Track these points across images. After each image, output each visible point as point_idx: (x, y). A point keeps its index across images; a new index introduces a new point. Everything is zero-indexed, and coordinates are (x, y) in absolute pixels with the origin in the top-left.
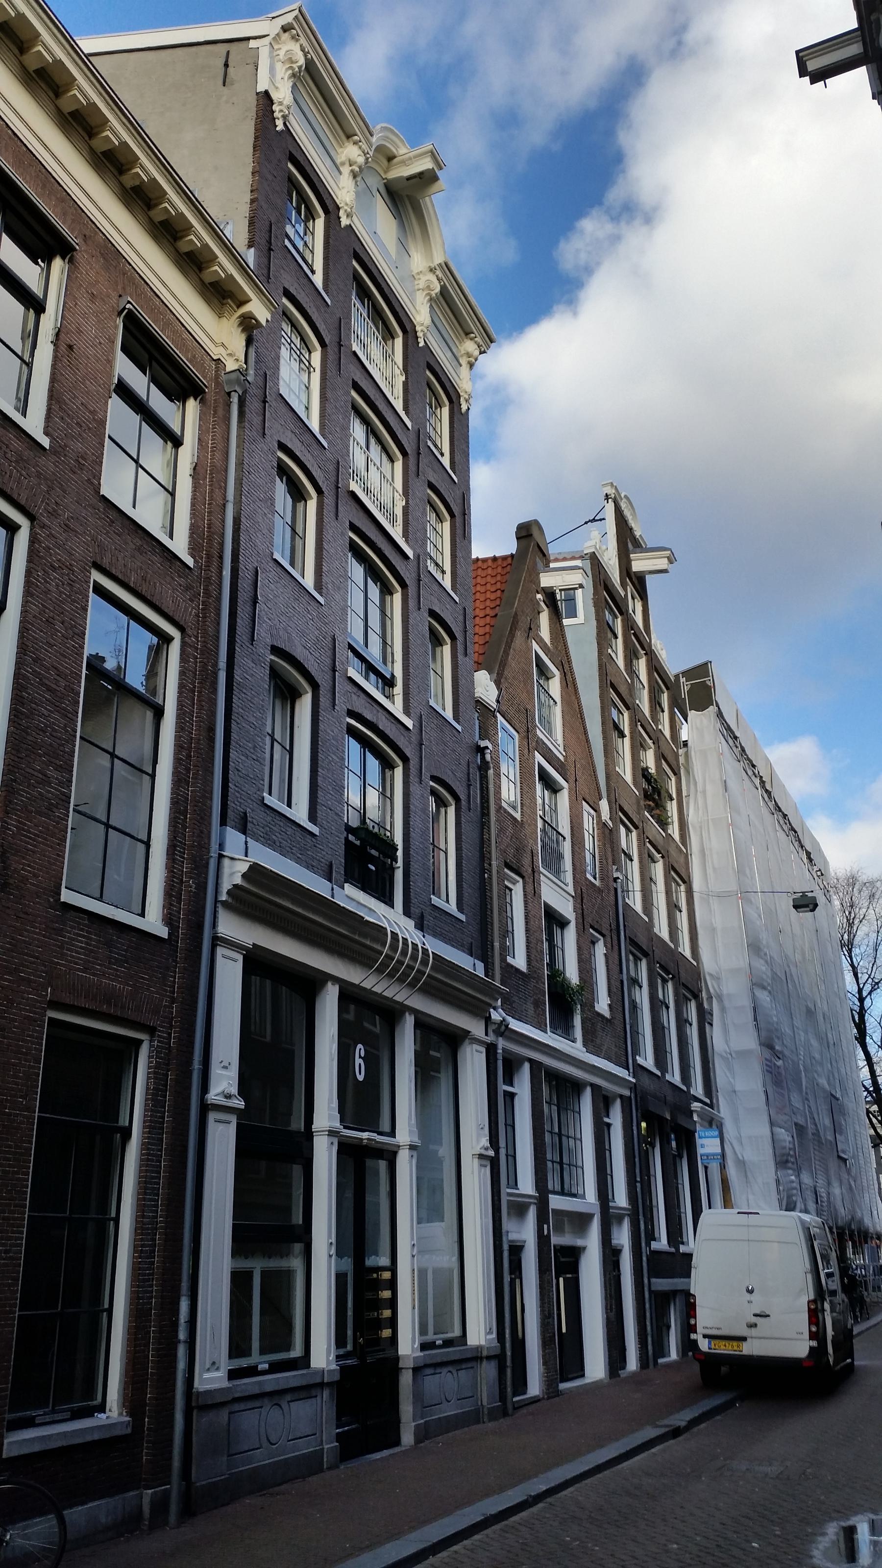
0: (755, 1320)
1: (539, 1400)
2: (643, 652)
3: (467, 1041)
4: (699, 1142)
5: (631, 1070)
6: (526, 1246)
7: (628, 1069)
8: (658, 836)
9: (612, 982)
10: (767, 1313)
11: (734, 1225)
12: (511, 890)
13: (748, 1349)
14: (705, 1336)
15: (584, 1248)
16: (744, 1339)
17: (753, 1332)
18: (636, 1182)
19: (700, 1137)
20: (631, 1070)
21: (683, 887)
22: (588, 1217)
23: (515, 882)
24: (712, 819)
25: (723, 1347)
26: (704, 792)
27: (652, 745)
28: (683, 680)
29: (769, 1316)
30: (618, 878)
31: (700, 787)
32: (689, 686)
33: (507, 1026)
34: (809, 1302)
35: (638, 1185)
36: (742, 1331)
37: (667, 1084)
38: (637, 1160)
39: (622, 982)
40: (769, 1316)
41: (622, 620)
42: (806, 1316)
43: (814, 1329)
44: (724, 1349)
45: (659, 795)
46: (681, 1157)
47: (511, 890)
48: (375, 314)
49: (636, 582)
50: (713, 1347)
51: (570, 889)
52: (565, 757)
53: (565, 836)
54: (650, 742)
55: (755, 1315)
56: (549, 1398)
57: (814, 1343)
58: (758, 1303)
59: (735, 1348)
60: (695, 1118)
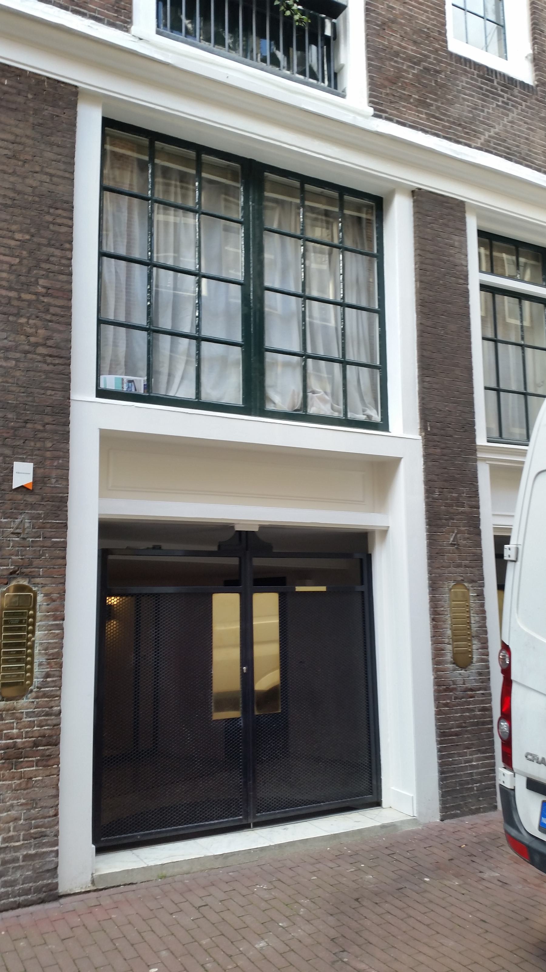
14: (533, 785)
15: (385, 532)
22: (381, 472)
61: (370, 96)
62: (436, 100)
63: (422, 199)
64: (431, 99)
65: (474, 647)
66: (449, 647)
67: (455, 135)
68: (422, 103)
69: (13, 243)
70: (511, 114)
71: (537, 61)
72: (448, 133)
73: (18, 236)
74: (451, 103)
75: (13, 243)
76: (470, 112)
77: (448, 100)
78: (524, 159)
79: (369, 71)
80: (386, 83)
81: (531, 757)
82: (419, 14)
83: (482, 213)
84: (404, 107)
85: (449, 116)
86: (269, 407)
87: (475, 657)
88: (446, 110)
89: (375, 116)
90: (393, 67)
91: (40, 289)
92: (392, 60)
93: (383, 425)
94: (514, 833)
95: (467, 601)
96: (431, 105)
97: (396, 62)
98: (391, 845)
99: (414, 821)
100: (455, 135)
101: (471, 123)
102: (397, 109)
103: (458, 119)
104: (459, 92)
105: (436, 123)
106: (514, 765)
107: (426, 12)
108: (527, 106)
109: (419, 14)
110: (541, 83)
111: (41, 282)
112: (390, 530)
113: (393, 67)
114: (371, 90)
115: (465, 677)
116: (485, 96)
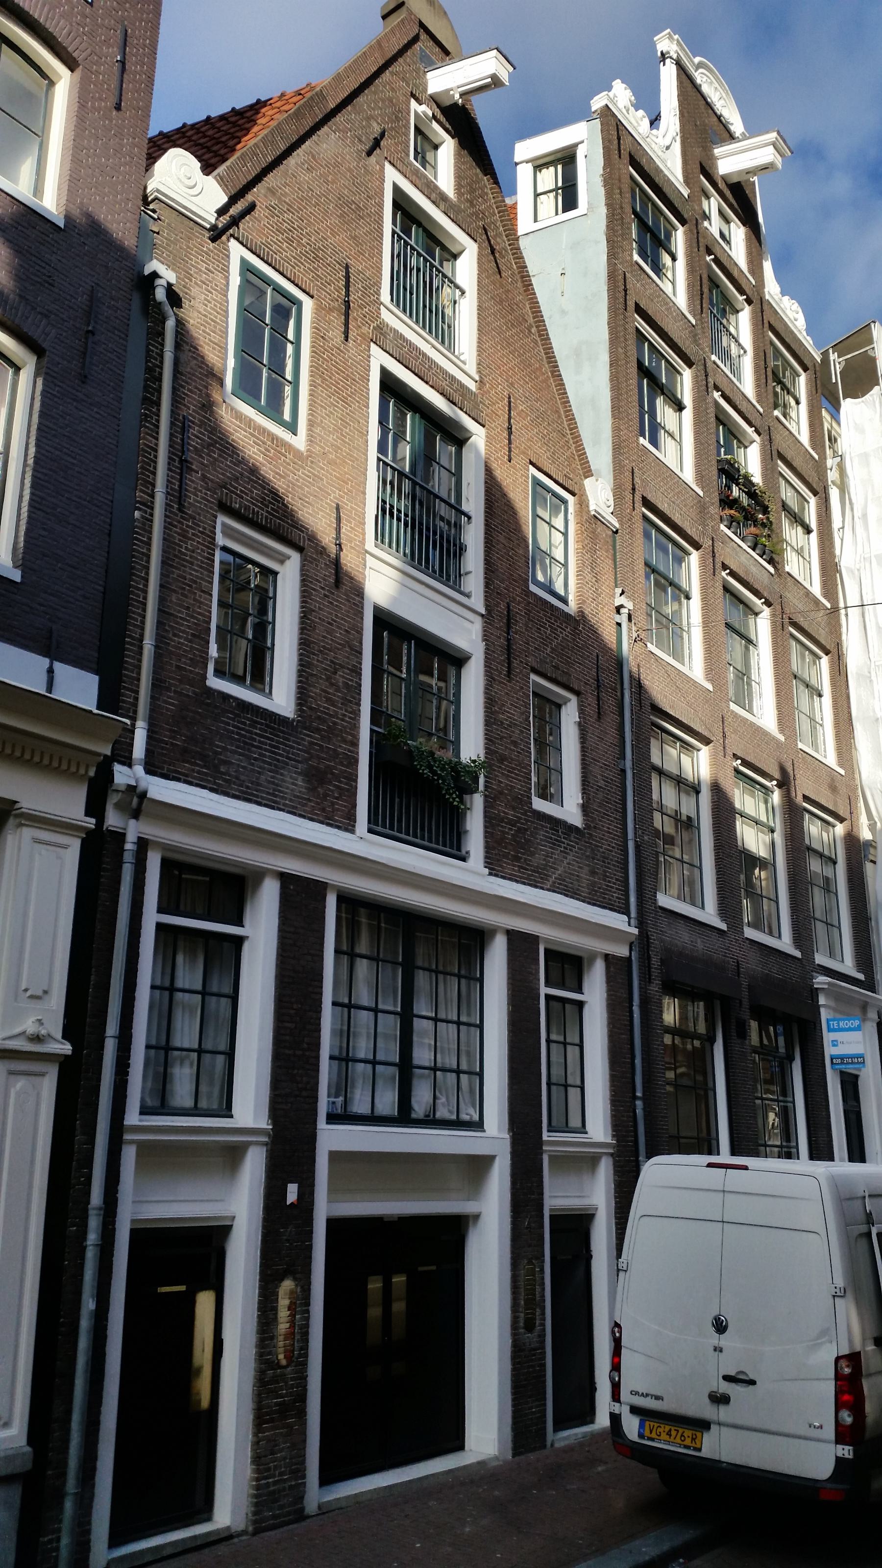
0: (725, 1387)
1: (230, 1537)
2: (742, 298)
3: (11, 822)
4: (828, 1037)
5: (633, 914)
6: (234, 1227)
7: (627, 913)
8: (754, 569)
9: (596, 770)
10: (752, 1377)
11: (685, 1188)
12: (275, 574)
13: (717, 1446)
14: (634, 1410)
15: (477, 1217)
16: (703, 1425)
17: (724, 1413)
18: (635, 1098)
19: (829, 1030)
20: (633, 914)
21: (825, 661)
22: (478, 1166)
23: (282, 559)
24: (876, 556)
25: (664, 1436)
26: (865, 516)
27: (755, 436)
28: (833, 356)
29: (752, 1382)
30: (622, 606)
31: (858, 513)
32: (843, 363)
33: (143, 795)
34: (838, 1359)
35: (639, 1104)
36: (704, 1410)
37: (747, 944)
38: (638, 1062)
39: (623, 771)
40: (752, 1382)
41: (685, 233)
42: (829, 1389)
43: (847, 1418)
44: (665, 1442)
45: (765, 510)
46: (791, 1059)
47: (275, 574)
48: (642, 195)
49: (728, 193)
50: (647, 1433)
51: (478, 602)
52: (481, 383)
53: (472, 514)
54: (750, 430)
55: (727, 1378)
56: (255, 1533)
57: (846, 1451)
58: (736, 1351)
59: (688, 1442)
60: (822, 1000)
61: (486, 857)
62: (524, 854)
63: (513, 936)
64: (521, 853)
65: (537, 1314)
66: (522, 1315)
67: (535, 881)
68: (517, 858)
69: (292, 1012)
70: (569, 857)
71: (585, 808)
72: (531, 880)
73: (295, 1006)
74: (532, 854)
75: (292, 1012)
76: (544, 860)
77: (531, 851)
78: (576, 894)
79: (486, 837)
80: (495, 845)
81: (634, 1393)
82: (516, 783)
83: (547, 941)
84: (505, 863)
85: (532, 866)
86: (414, 1116)
87: (538, 1322)
88: (530, 860)
89: (490, 874)
90: (500, 831)
91: (305, 1046)
92: (499, 825)
93: (478, 1125)
94: (620, 1441)
95: (534, 1275)
96: (521, 858)
97: (502, 827)
98: (482, 1475)
99: (496, 1458)
100: (535, 881)
101: (544, 869)
102: (501, 866)
103: (537, 867)
104: (538, 844)
105: (524, 873)
106: (622, 1399)
107: (520, 781)
108: (579, 848)
109: (516, 783)
110: (587, 827)
111: (306, 1040)
112: (482, 1216)
113: (500, 831)
114: (486, 852)
115: (530, 1338)
116: (555, 843)
